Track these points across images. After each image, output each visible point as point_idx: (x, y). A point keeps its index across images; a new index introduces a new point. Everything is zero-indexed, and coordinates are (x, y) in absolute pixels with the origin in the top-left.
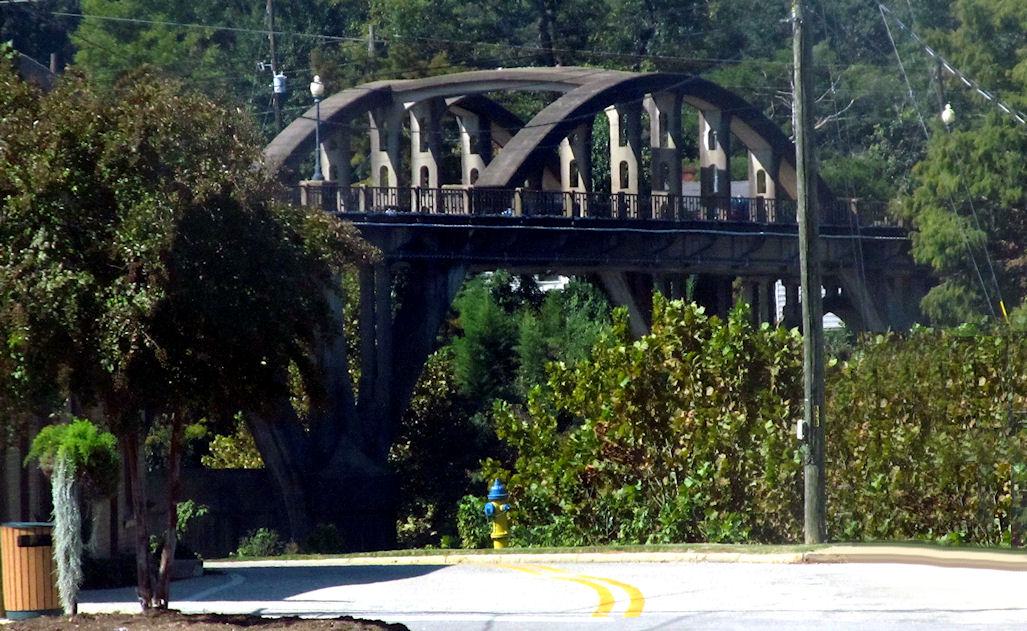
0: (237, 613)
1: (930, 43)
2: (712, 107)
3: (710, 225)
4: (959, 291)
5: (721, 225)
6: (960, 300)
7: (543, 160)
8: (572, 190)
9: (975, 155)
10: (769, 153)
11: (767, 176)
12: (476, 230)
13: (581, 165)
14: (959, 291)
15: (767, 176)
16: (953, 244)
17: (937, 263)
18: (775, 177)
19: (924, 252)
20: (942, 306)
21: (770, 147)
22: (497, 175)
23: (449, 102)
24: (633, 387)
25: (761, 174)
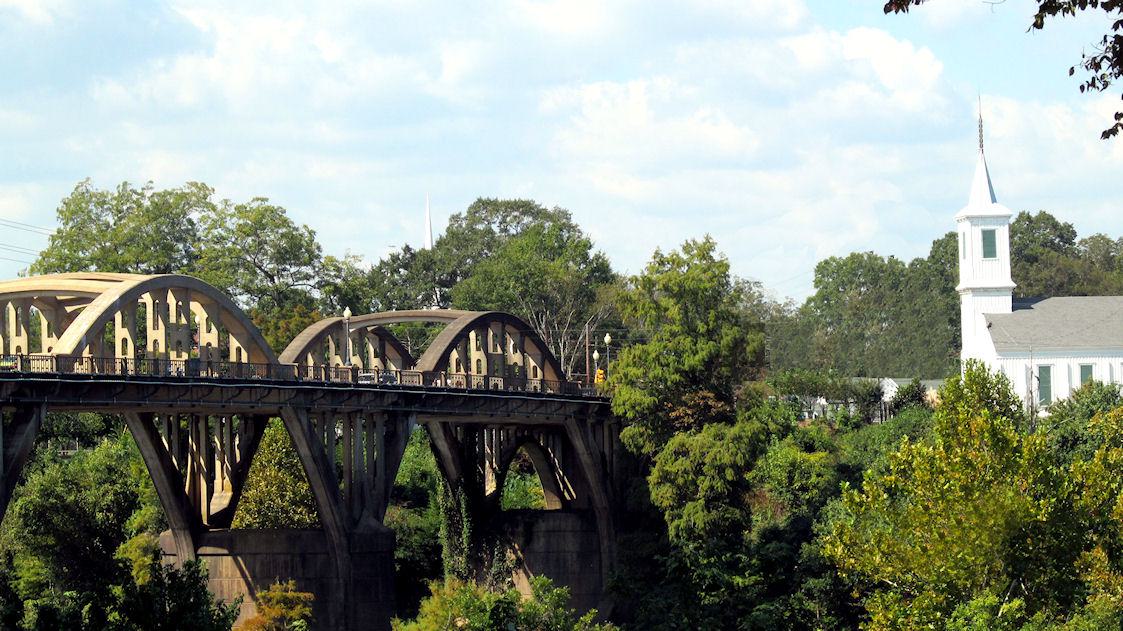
0: (979, 286)
1: (949, 568)
2: (516, 331)
3: (507, 393)
4: (642, 429)
5: (550, 395)
6: (642, 435)
7: (100, 331)
8: (124, 350)
9: (650, 357)
10: (539, 357)
11: (538, 369)
12: (427, 395)
13: (463, 360)
14: (642, 429)
15: (538, 369)
16: (640, 404)
17: (630, 415)
18: (542, 370)
19: (618, 411)
20: (632, 437)
21: (539, 352)
22: (427, 365)
23: (369, 329)
24: (405, 504)
25: (535, 368)
